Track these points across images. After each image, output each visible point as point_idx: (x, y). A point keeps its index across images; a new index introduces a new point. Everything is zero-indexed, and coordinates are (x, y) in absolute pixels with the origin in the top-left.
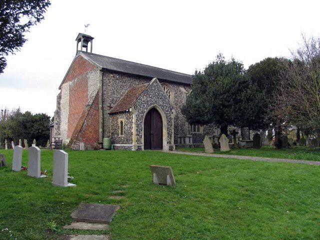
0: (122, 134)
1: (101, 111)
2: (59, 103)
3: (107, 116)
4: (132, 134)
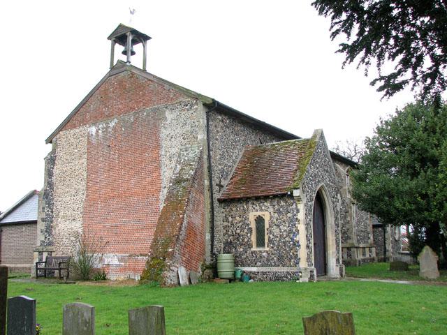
0: (261, 243)
1: (207, 193)
2: (49, 174)
3: (216, 204)
4: (296, 244)
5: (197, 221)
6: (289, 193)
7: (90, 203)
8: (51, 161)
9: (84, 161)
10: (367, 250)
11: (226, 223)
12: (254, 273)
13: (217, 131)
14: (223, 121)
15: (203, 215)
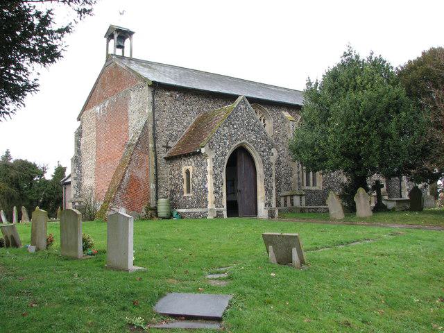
0: (188, 191)
1: (152, 153)
2: (78, 144)
3: (162, 162)
5: (140, 174)
6: (198, 151)
7: (98, 164)
8: (79, 134)
9: (95, 133)
10: (289, 198)
11: (171, 176)
12: (184, 213)
13: (165, 105)
14: (171, 96)
15: (148, 170)
